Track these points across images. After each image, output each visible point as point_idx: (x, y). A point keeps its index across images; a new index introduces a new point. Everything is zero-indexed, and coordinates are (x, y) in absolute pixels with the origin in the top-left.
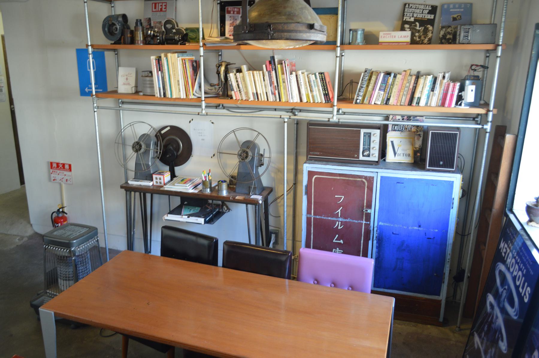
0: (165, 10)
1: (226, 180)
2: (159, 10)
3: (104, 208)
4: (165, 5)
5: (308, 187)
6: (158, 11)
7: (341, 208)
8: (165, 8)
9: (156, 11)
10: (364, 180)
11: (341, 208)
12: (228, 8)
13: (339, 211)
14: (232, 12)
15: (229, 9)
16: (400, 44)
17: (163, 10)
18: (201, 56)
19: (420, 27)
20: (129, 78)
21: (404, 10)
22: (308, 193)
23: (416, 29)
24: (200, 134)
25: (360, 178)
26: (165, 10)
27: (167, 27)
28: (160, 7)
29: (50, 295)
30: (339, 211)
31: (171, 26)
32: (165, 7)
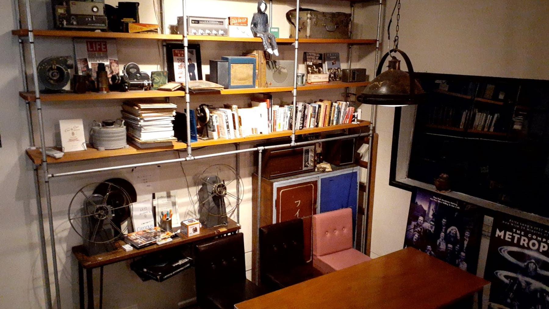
0: (105, 50)
1: (181, 222)
2: (97, 49)
3: (356, 236)
4: (104, 45)
5: (277, 201)
6: (96, 51)
7: (299, 210)
8: (104, 48)
9: (93, 51)
10: (312, 184)
11: (299, 210)
12: (175, 51)
13: (298, 213)
14: (179, 55)
15: (176, 51)
16: (314, 83)
17: (103, 50)
18: (187, 102)
19: (316, 68)
20: (75, 132)
21: (306, 57)
22: (277, 206)
23: (314, 71)
24: (146, 181)
25: (309, 184)
26: (105, 50)
27: (130, 72)
28: (98, 47)
29: (535, 232)
30: (298, 213)
31: (135, 70)
32: (104, 47)
